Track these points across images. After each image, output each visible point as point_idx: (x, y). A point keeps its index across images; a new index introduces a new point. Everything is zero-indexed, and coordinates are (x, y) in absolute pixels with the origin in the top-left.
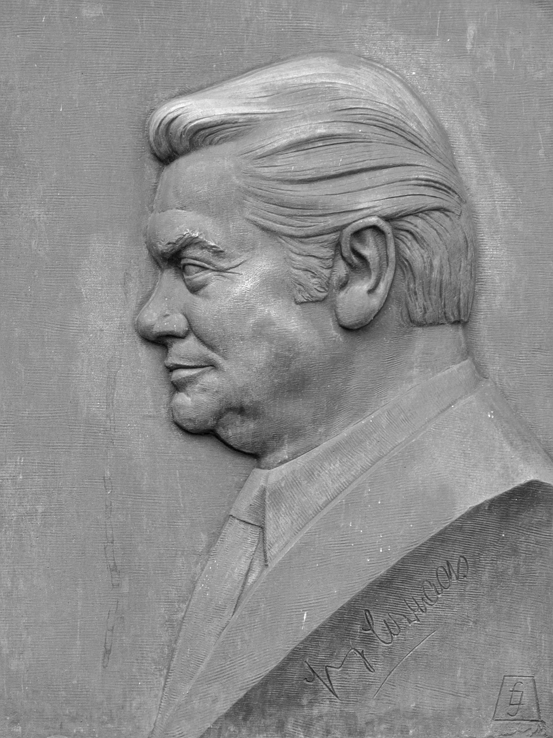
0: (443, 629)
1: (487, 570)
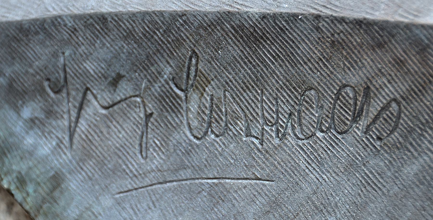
0: (286, 189)
1: (421, 160)
